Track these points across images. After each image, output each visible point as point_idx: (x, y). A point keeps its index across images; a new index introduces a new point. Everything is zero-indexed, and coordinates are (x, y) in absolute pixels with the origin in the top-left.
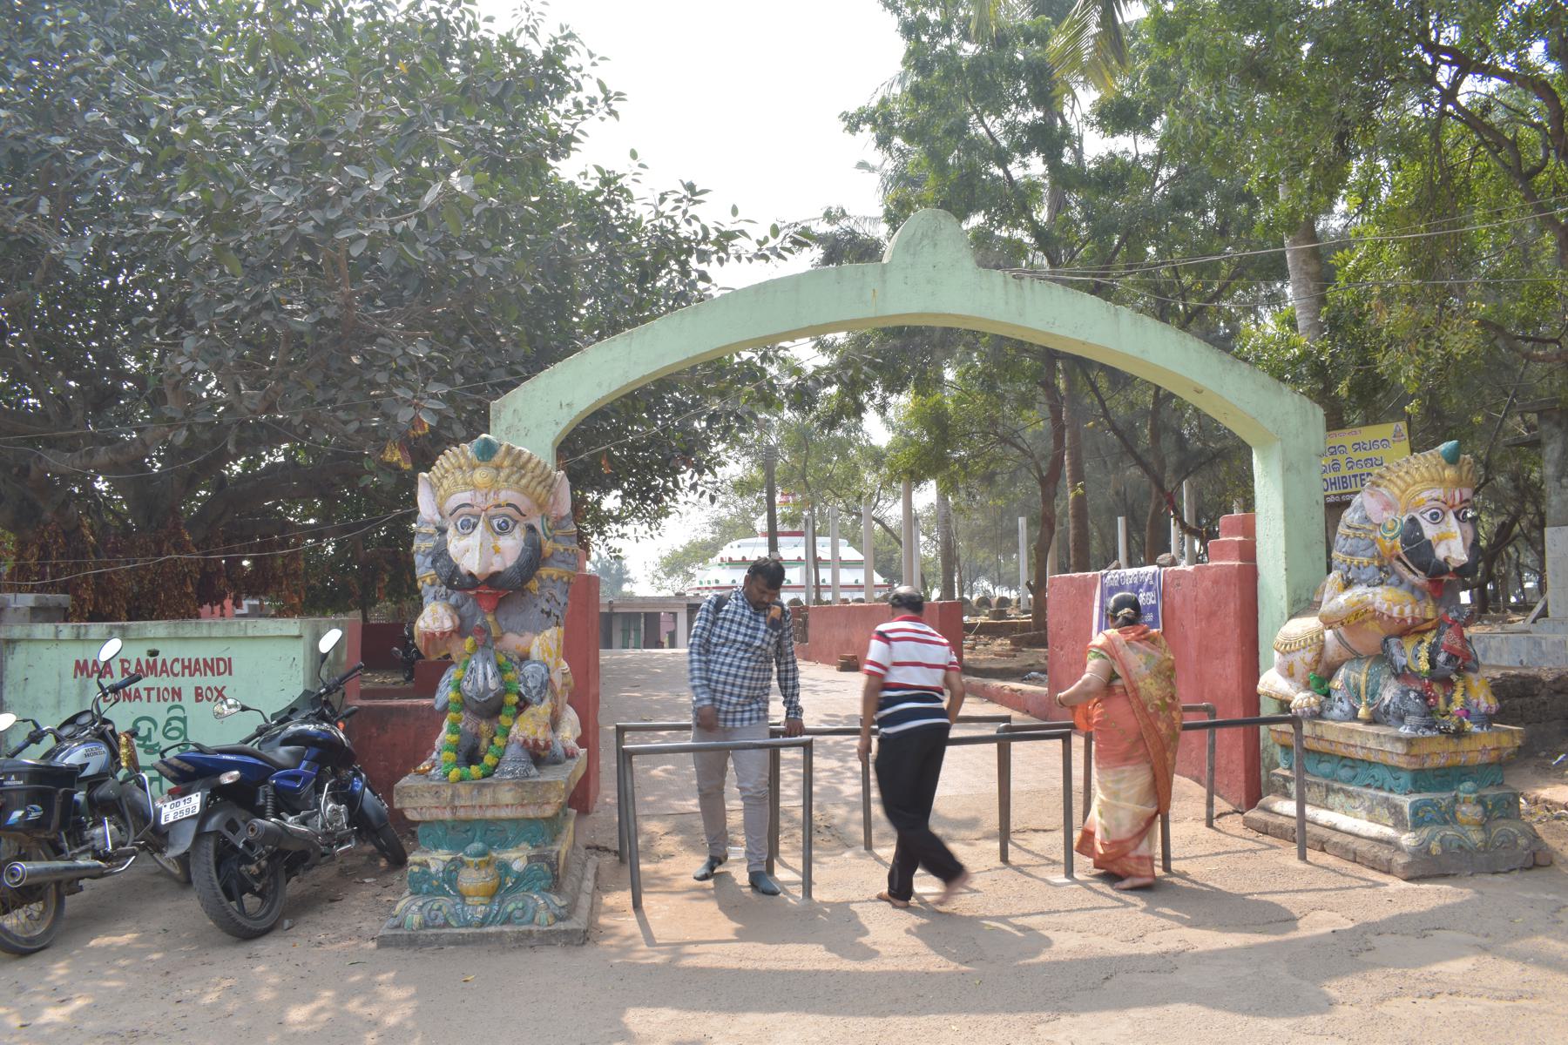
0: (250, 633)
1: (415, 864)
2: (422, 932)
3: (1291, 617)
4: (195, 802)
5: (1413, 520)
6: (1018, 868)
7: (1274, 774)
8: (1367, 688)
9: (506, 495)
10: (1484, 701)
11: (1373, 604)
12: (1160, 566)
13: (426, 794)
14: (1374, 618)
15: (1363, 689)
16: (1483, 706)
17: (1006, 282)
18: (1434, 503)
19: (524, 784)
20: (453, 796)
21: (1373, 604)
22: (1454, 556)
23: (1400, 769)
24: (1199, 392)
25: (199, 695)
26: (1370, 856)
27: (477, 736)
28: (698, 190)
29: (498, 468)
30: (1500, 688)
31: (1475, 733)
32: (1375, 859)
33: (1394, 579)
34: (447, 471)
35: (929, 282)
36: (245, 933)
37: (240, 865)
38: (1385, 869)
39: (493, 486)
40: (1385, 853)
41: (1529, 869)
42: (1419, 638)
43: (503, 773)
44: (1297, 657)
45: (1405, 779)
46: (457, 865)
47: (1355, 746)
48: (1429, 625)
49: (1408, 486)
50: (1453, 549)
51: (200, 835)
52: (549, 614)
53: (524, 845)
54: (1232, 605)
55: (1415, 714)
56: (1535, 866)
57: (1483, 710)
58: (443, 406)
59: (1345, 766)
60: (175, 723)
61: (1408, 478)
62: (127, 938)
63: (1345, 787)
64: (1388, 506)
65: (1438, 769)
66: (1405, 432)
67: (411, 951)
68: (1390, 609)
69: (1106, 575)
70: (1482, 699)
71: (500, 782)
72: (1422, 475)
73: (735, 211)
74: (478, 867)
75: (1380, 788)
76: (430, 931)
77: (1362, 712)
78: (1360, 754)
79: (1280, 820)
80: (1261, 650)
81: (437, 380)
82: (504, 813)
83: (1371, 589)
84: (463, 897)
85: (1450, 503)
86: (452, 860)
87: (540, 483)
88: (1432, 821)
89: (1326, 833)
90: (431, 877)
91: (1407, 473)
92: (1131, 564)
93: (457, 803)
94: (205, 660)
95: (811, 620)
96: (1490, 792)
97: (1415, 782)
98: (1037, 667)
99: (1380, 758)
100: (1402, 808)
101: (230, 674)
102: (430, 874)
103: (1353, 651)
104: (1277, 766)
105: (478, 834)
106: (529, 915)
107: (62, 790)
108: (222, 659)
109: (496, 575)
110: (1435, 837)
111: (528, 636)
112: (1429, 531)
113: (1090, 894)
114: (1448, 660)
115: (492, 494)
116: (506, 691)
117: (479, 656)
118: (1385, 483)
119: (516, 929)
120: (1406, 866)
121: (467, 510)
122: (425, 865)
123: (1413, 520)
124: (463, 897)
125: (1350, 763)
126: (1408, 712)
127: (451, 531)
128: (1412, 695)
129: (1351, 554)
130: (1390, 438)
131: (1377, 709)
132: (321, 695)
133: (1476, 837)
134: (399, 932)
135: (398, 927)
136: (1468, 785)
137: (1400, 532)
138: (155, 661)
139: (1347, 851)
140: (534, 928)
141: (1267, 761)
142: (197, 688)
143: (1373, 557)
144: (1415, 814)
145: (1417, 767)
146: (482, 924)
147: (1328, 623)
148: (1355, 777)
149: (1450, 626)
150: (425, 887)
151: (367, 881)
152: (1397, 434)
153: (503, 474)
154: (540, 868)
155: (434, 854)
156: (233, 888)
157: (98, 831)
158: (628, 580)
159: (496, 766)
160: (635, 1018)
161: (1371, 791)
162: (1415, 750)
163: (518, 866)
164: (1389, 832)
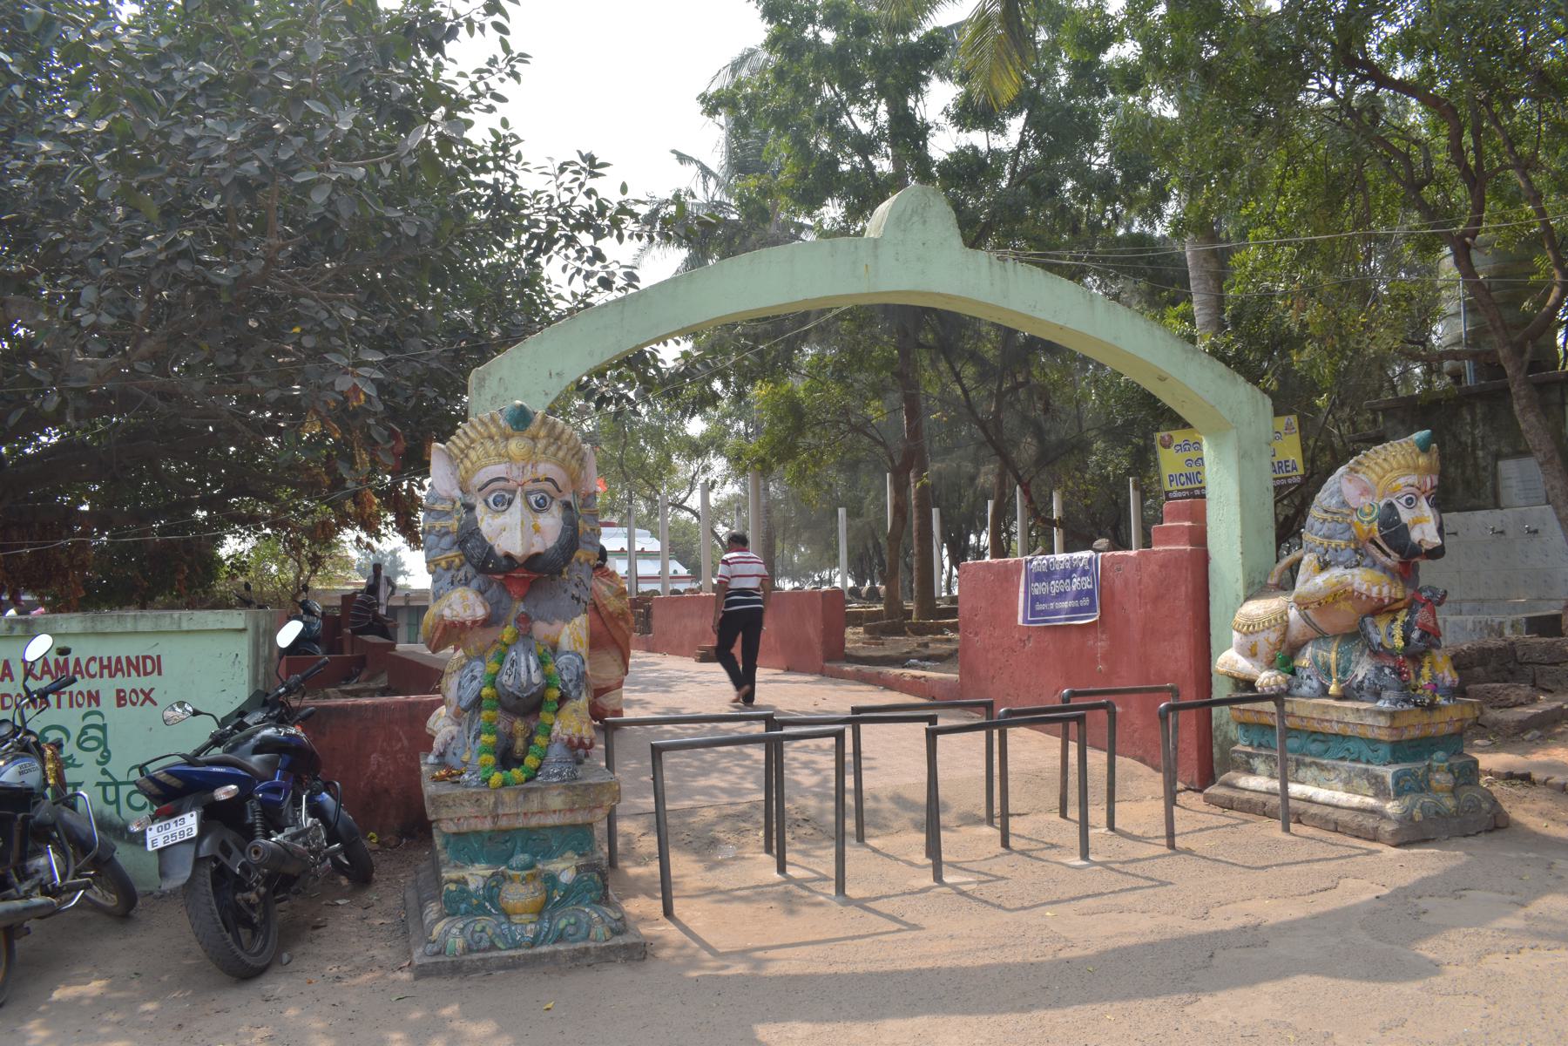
0: (185, 626)
1: (451, 881)
2: (468, 957)
3: (1247, 599)
4: (189, 823)
5: (1390, 505)
6: (1022, 853)
7: (1235, 751)
8: (1338, 665)
9: (545, 469)
10: (1449, 676)
11: (1352, 584)
12: (1097, 551)
13: (466, 803)
14: (1346, 599)
15: (1333, 667)
16: (1448, 680)
17: (991, 263)
18: (1409, 489)
19: (574, 787)
20: (496, 803)
21: (1352, 584)
22: (1428, 539)
23: (1378, 741)
24: (1162, 379)
25: (121, 699)
26: (1354, 825)
27: (511, 736)
28: (597, 162)
29: (534, 438)
30: (1461, 662)
31: (1444, 706)
32: (1361, 828)
33: (1368, 561)
34: (473, 441)
35: (918, 259)
36: (244, 973)
37: (235, 894)
38: (1371, 837)
39: (531, 458)
40: (1370, 822)
41: (1490, 831)
42: (1391, 617)
43: (548, 776)
44: (1261, 638)
45: (1384, 751)
46: (499, 880)
47: (1331, 721)
48: (1401, 604)
49: (1386, 472)
50: (1426, 531)
51: (198, 861)
52: (578, 600)
53: (569, 854)
54: (1183, 588)
55: (1391, 689)
56: (1496, 828)
57: (1447, 684)
58: (381, 376)
59: (1314, 741)
60: (92, 732)
61: (1386, 466)
62: (95, 987)
63: (1317, 760)
64: (1365, 491)
65: (1411, 740)
66: (1296, 425)
67: (456, 979)
68: (1369, 589)
69: (1031, 561)
70: (1447, 673)
71: (547, 787)
72: (1399, 463)
73: (624, 189)
74: (525, 881)
75: (1357, 760)
76: (476, 956)
77: (1333, 689)
78: (1336, 728)
79: (1247, 795)
80: (1213, 632)
81: (371, 347)
82: (552, 820)
83: (1348, 571)
84: (507, 915)
85: (1423, 489)
86: (493, 875)
87: (573, 456)
88: (1411, 790)
89: (1302, 806)
90: (470, 895)
91: (1385, 460)
92: (1067, 549)
93: (500, 811)
94: (128, 659)
95: (656, 612)
96: (1456, 761)
97: (1393, 753)
98: (914, 654)
99: (1359, 731)
100: (1383, 778)
101: (160, 673)
102: (468, 892)
103: (1318, 630)
104: (1235, 743)
105: (519, 844)
106: (583, 931)
107: (20, 816)
108: (149, 657)
109: (538, 555)
110: (1417, 803)
111: (558, 623)
112: (1406, 516)
113: (1115, 875)
114: (1422, 637)
115: (529, 467)
116: (548, 686)
117: (520, 647)
118: (1364, 469)
119: (571, 947)
120: (1394, 833)
121: (501, 484)
122: (462, 882)
123: (1390, 505)
124: (507, 915)
125: (1322, 738)
126: (1386, 688)
127: (480, 509)
128: (1387, 671)
129: (1329, 537)
130: (1282, 431)
131: (1349, 686)
132: (280, 695)
133: (1449, 803)
134: (440, 959)
135: (438, 953)
136: (1440, 755)
137: (1378, 516)
138: (66, 661)
139: (1327, 821)
140: (591, 945)
141: (1220, 739)
142: (119, 691)
143: (1349, 540)
144: (1396, 783)
145: (1395, 739)
146: (533, 944)
147: (1303, 604)
148: (1326, 751)
149: (1423, 605)
150: (463, 906)
151: (340, 902)
152: (1288, 427)
153: (541, 445)
154: (590, 879)
155: (472, 869)
156: (236, 919)
157: (42, 861)
158: (404, 573)
159: (537, 769)
160: (764, 1032)
161: (1347, 763)
162: (1397, 724)
163: (567, 877)
164: (1371, 802)
